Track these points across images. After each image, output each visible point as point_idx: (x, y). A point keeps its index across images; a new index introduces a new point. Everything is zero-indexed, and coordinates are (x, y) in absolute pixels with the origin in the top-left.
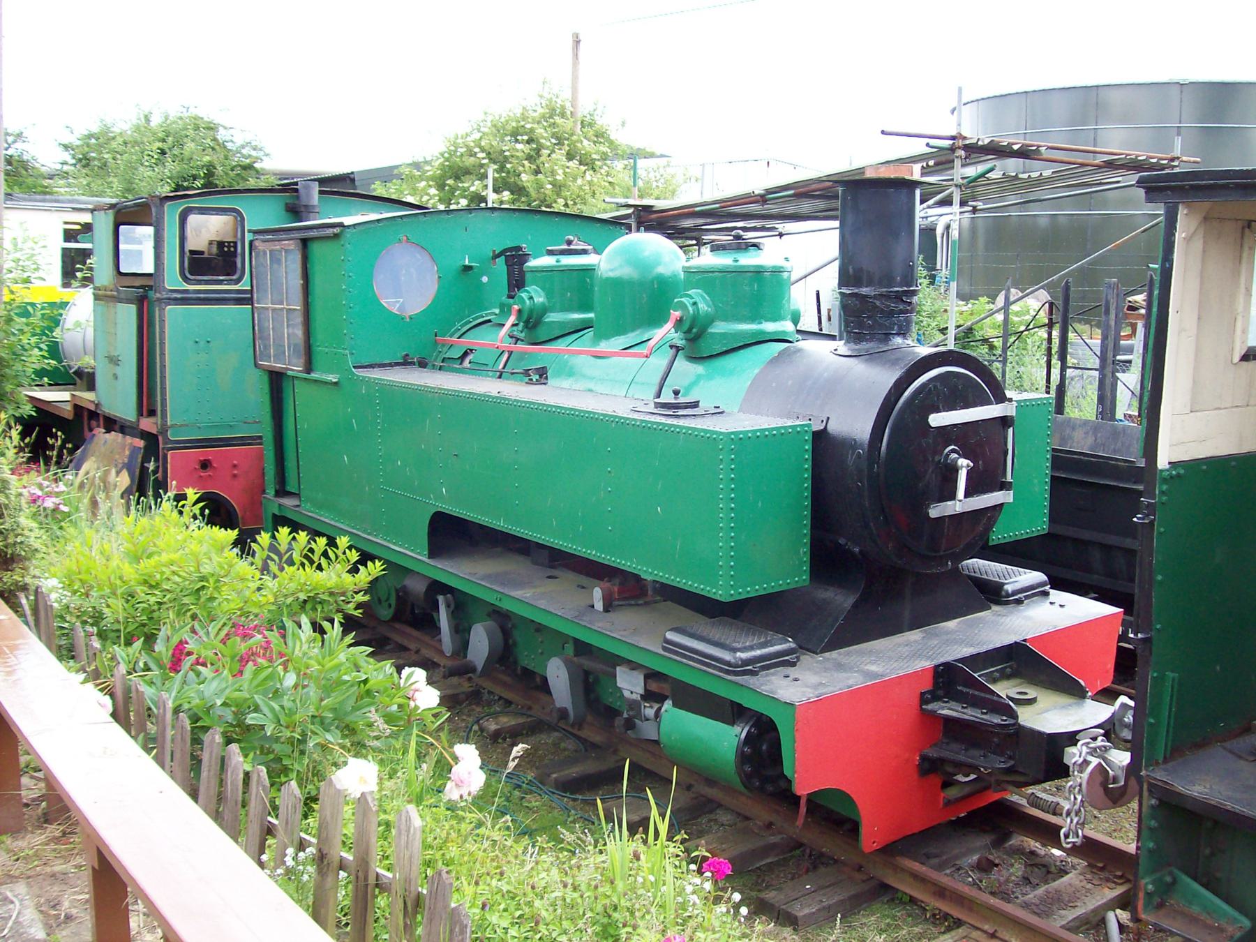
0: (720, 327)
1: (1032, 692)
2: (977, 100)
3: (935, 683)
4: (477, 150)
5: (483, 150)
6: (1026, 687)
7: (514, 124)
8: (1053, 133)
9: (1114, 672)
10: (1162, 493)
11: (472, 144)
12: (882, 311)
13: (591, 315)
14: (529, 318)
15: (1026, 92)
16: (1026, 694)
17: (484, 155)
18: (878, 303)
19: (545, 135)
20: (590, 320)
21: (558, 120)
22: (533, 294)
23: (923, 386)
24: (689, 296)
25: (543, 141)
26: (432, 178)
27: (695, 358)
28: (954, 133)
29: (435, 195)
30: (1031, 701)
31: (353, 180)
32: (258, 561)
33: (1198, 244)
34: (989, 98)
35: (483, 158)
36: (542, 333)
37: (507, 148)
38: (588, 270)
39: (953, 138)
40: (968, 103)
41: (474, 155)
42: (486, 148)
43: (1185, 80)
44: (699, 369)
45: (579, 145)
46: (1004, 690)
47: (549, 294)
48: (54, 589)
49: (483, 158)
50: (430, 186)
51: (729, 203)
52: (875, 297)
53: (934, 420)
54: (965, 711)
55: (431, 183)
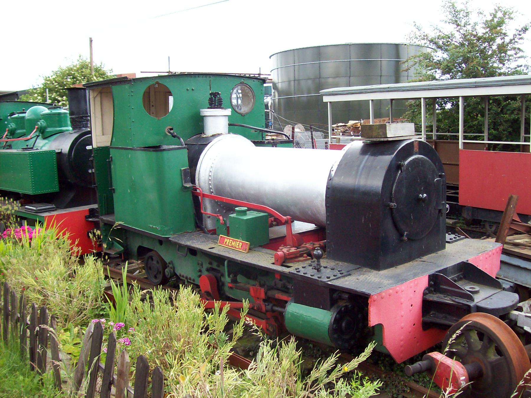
0: (49, 129)
1: (477, 288)
2: (277, 53)
3: (90, 214)
4: (54, 82)
5: (56, 82)
6: (474, 285)
7: (67, 72)
8: (353, 62)
9: (457, 264)
10: (95, 153)
11: (52, 80)
12: (78, 122)
13: (25, 131)
14: (11, 132)
15: (294, 50)
16: (470, 288)
17: (57, 84)
18: (76, 119)
19: (79, 75)
20: (25, 132)
21: (84, 70)
22: (12, 125)
23: (84, 139)
24: (40, 122)
25: (78, 78)
26: (39, 93)
27: (45, 138)
28: (168, 71)
29: (40, 99)
30: (477, 292)
31: (17, 95)
32: (51, 258)
33: (98, 99)
34: (283, 52)
35: (57, 85)
36: (16, 136)
37: (65, 81)
38: (24, 117)
39: (167, 72)
40: (274, 54)
41: (53, 84)
42: (57, 81)
43: (350, 43)
44: (46, 141)
45: (92, 79)
46: (467, 287)
47: (17, 124)
48: (65, 342)
49: (57, 85)
50: (39, 96)
51: (368, 91)
52: (76, 118)
53: (88, 147)
54: (446, 298)
55: (39, 95)
